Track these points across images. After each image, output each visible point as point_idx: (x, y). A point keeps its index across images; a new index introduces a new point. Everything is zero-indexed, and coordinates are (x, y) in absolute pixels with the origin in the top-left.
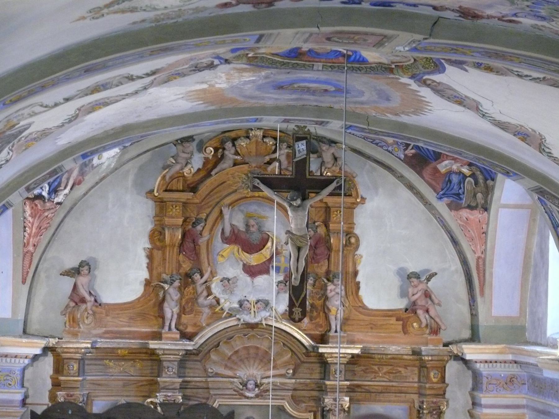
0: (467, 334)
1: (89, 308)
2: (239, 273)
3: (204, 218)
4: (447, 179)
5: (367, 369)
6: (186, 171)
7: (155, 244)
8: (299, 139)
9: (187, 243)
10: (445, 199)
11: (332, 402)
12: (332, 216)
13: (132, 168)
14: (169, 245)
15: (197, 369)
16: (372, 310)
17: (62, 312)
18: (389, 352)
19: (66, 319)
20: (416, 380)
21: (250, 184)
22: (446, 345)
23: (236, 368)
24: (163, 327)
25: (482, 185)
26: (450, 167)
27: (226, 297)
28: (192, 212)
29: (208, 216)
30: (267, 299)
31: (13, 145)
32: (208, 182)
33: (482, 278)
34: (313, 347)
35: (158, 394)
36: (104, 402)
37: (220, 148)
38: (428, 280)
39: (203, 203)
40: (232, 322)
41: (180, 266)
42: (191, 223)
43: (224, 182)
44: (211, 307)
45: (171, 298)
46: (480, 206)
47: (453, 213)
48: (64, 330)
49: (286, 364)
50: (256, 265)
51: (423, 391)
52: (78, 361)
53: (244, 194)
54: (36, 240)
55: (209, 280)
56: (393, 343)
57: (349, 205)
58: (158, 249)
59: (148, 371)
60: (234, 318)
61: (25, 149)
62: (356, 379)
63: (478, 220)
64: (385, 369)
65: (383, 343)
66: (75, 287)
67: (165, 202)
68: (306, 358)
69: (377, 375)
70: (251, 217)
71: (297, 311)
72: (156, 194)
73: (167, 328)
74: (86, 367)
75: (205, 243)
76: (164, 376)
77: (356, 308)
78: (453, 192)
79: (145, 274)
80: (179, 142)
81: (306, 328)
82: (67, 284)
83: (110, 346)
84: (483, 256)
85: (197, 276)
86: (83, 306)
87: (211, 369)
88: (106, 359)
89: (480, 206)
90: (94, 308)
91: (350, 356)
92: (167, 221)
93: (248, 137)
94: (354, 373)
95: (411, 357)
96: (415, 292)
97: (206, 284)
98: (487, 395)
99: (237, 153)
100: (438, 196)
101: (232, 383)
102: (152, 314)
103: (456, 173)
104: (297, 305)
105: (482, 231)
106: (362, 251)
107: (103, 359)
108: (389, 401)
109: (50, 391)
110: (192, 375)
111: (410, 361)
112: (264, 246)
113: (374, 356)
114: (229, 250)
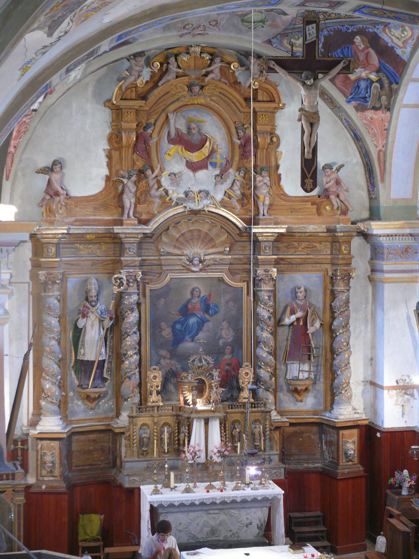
0: (366, 214)
1: (62, 200)
2: (183, 169)
3: (153, 122)
4: (356, 85)
5: (289, 245)
6: (139, 82)
7: (113, 146)
8: (309, 23)
9: (139, 144)
10: (353, 102)
11: (263, 272)
12: (258, 120)
13: (91, 80)
14: (126, 146)
15: (151, 249)
16: (292, 197)
17: (38, 205)
18: (308, 231)
19: (43, 209)
20: (329, 252)
21: (265, 66)
22: (353, 223)
23: (182, 247)
24: (122, 214)
25: (387, 89)
26: (359, 74)
27: (174, 188)
28: (143, 118)
29: (156, 121)
30: (207, 189)
31: (75, 14)
32: (156, 92)
33: (382, 168)
34: (246, 228)
35: (122, 271)
36: (76, 279)
37: (165, 62)
38: (338, 170)
39: (151, 110)
40: (180, 209)
41: (134, 163)
42: (143, 127)
43: (169, 92)
44: (161, 197)
45: (129, 190)
46: (383, 107)
47: (359, 114)
48: (42, 220)
49: (223, 244)
50: (197, 162)
51: (336, 262)
52: (55, 245)
53: (186, 102)
54: (16, 142)
55: (158, 175)
56: (310, 224)
57: (272, 109)
58: (116, 150)
59: (112, 252)
60: (182, 206)
61: (85, 19)
62: (280, 253)
63: (381, 119)
64: (304, 245)
65: (302, 223)
66: (49, 182)
67: (121, 109)
68: (239, 237)
69: (297, 250)
70: (191, 122)
71: (309, 181)
72: (115, 102)
73: (126, 216)
74: (61, 250)
75: (155, 143)
76: (126, 255)
77: (279, 196)
78: (361, 95)
79: (105, 171)
80: (132, 57)
81: (238, 213)
82: (42, 181)
83: (80, 232)
84: (383, 149)
85: (149, 172)
86: (57, 199)
87: (163, 249)
88: (77, 243)
89: (383, 107)
90: (66, 200)
91: (277, 235)
92: (124, 125)
93: (188, 53)
94: (278, 249)
95: (325, 234)
96: (329, 180)
97: (157, 178)
98: (388, 263)
99: (179, 67)
100: (347, 100)
101: (180, 260)
102: (113, 204)
103: (364, 80)
104: (309, 176)
105: (384, 128)
106: (282, 148)
107: (75, 243)
108: (307, 271)
109: (31, 272)
110: (147, 254)
111: (323, 238)
112: (203, 146)
113: (294, 234)
114: (174, 149)
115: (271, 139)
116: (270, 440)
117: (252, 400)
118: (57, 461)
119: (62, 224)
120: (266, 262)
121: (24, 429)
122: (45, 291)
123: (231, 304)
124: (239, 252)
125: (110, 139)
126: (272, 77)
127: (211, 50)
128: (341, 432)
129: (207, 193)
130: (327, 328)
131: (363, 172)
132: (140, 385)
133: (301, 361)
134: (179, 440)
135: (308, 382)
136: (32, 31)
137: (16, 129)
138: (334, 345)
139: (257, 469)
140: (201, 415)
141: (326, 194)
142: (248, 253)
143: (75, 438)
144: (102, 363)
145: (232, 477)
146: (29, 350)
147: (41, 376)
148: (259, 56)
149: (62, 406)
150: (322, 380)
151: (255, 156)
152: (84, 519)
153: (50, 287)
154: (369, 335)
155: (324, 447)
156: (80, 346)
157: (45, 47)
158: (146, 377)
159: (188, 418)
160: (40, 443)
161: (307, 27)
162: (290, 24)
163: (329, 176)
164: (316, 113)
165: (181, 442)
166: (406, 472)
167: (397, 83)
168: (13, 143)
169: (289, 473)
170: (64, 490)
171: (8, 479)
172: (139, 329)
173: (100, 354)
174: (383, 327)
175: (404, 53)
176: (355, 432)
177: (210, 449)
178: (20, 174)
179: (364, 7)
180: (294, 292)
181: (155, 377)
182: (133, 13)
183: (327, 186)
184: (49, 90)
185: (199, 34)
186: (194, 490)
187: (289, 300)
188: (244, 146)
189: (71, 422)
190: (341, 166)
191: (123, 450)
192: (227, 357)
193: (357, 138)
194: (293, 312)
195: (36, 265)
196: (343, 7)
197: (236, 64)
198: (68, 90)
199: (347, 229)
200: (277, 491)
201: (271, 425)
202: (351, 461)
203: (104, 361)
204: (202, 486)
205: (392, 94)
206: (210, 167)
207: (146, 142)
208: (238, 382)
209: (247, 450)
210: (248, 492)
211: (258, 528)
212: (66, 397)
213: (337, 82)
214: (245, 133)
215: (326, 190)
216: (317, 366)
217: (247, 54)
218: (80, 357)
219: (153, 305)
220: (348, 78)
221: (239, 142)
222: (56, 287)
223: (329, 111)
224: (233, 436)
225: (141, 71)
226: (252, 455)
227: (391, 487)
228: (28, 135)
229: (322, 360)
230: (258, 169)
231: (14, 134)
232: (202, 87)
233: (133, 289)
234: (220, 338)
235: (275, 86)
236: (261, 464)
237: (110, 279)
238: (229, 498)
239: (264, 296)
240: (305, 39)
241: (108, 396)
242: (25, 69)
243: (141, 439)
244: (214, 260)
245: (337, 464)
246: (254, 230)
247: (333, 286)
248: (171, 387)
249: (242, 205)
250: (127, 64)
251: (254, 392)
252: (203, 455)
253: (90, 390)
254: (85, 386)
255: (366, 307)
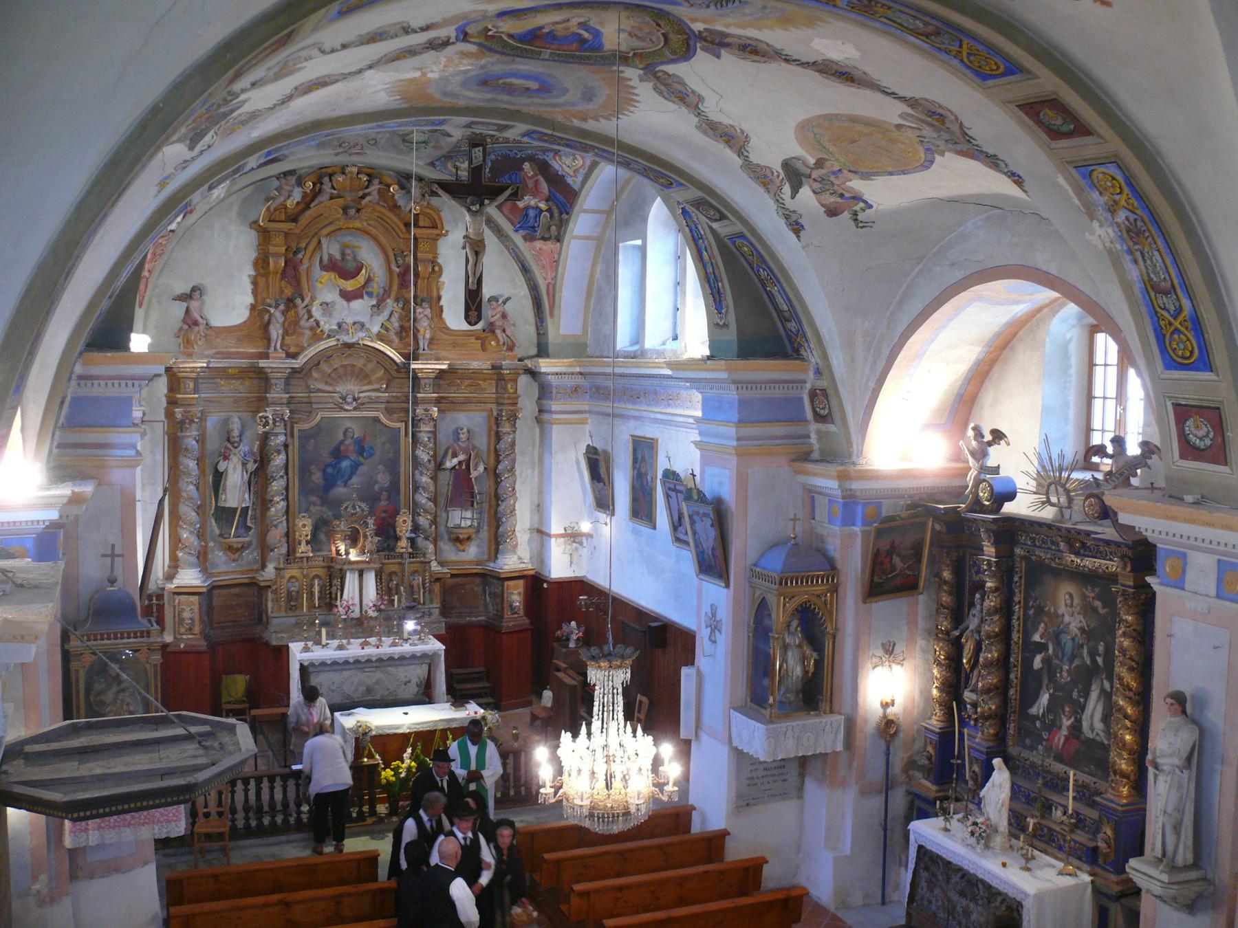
0: (534, 351)
6: (289, 203)
8: (475, 145)
11: (423, 412)
19: (180, 340)
22: (520, 360)
27: (326, 319)
29: (307, 245)
32: (308, 214)
34: (404, 364)
37: (318, 182)
38: (504, 303)
40: (332, 342)
41: (282, 292)
44: (311, 329)
47: (527, 244)
49: (379, 380)
56: (474, 360)
58: (262, 276)
64: (467, 382)
66: (188, 310)
71: (473, 314)
73: (272, 349)
82: (179, 309)
85: (298, 301)
86: (196, 329)
92: (272, 249)
93: (343, 173)
94: (439, 386)
99: (333, 188)
101: (332, 397)
103: (533, 208)
104: (473, 308)
106: (445, 278)
109: (166, 409)
115: (433, 269)
116: (430, 592)
117: (410, 550)
118: (197, 618)
119: (202, 356)
120: (425, 401)
121: (159, 582)
122: (182, 431)
123: (388, 445)
124: (396, 390)
125: (256, 264)
126: (435, 201)
127: (369, 171)
128: (506, 583)
129: (363, 325)
130: (492, 473)
131: (531, 306)
132: (287, 534)
133: (464, 507)
134: (330, 593)
135: (471, 530)
136: (172, 144)
137: (151, 251)
138: (499, 491)
139: (417, 624)
140: (355, 566)
141: (491, 328)
142: (406, 390)
143: (216, 592)
144: (245, 511)
145: (389, 632)
146: (165, 495)
147: (177, 525)
148: (420, 179)
149: (201, 558)
150: (486, 528)
151: (415, 285)
152: (227, 680)
153: (187, 426)
154: (536, 480)
155: (488, 599)
156: (221, 491)
157: (185, 161)
158: (294, 525)
159: (341, 570)
160: (177, 598)
161: (473, 150)
162: (455, 146)
163: (495, 309)
164: (482, 242)
165: (334, 596)
166: (573, 624)
167: (567, 213)
168: (147, 266)
169: (449, 627)
170: (204, 648)
171: (142, 637)
172: (287, 474)
173: (244, 500)
174: (551, 471)
175: (575, 182)
176: (521, 582)
177: (364, 602)
178: (154, 301)
179: (534, 132)
180: (456, 433)
181: (304, 526)
182: (284, 128)
183: (492, 320)
184: (189, 209)
185: (357, 153)
186: (348, 647)
187: (451, 441)
188: (404, 275)
189: (212, 575)
190: (508, 299)
191: (270, 605)
192: (383, 503)
193: (525, 270)
194: (455, 455)
195: (172, 402)
196: (511, 131)
197: (396, 187)
198: (210, 209)
199: (513, 367)
200: (438, 646)
201: (431, 576)
202: (516, 613)
203: (247, 508)
204: (356, 642)
205: (562, 224)
206: (365, 297)
207: (296, 269)
208: (395, 531)
209: (404, 603)
210: (406, 648)
211: (417, 685)
212: (206, 547)
213: (504, 209)
214: (404, 261)
215: (492, 324)
216: (481, 513)
217: (407, 176)
218: (221, 504)
219: (303, 447)
220: (516, 206)
221: (397, 270)
222: (194, 426)
223: (496, 240)
224: (389, 589)
225: (292, 191)
226: (411, 608)
227: (559, 639)
228: (165, 257)
229: (486, 507)
230: (419, 300)
231: (149, 256)
232: (358, 211)
233: (280, 429)
234: (376, 482)
235: (438, 211)
236: (420, 618)
237: (254, 417)
238: (385, 654)
239: (424, 437)
240: (471, 162)
241: (253, 547)
242: (162, 184)
243: (289, 593)
244: (370, 398)
245: (502, 617)
246: (413, 366)
247: (498, 427)
248: (322, 536)
249: (401, 339)
250: (276, 183)
251: (412, 541)
252: (357, 610)
253: (232, 540)
254: (226, 536)
255: (533, 450)
